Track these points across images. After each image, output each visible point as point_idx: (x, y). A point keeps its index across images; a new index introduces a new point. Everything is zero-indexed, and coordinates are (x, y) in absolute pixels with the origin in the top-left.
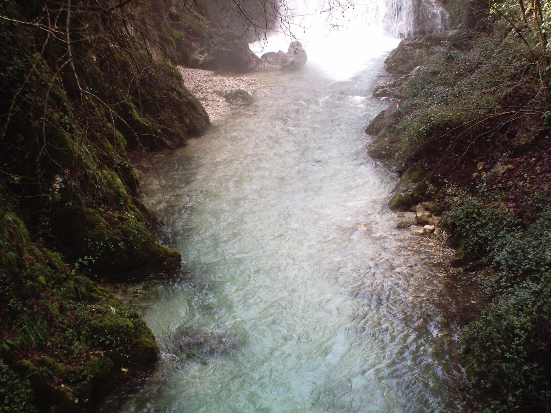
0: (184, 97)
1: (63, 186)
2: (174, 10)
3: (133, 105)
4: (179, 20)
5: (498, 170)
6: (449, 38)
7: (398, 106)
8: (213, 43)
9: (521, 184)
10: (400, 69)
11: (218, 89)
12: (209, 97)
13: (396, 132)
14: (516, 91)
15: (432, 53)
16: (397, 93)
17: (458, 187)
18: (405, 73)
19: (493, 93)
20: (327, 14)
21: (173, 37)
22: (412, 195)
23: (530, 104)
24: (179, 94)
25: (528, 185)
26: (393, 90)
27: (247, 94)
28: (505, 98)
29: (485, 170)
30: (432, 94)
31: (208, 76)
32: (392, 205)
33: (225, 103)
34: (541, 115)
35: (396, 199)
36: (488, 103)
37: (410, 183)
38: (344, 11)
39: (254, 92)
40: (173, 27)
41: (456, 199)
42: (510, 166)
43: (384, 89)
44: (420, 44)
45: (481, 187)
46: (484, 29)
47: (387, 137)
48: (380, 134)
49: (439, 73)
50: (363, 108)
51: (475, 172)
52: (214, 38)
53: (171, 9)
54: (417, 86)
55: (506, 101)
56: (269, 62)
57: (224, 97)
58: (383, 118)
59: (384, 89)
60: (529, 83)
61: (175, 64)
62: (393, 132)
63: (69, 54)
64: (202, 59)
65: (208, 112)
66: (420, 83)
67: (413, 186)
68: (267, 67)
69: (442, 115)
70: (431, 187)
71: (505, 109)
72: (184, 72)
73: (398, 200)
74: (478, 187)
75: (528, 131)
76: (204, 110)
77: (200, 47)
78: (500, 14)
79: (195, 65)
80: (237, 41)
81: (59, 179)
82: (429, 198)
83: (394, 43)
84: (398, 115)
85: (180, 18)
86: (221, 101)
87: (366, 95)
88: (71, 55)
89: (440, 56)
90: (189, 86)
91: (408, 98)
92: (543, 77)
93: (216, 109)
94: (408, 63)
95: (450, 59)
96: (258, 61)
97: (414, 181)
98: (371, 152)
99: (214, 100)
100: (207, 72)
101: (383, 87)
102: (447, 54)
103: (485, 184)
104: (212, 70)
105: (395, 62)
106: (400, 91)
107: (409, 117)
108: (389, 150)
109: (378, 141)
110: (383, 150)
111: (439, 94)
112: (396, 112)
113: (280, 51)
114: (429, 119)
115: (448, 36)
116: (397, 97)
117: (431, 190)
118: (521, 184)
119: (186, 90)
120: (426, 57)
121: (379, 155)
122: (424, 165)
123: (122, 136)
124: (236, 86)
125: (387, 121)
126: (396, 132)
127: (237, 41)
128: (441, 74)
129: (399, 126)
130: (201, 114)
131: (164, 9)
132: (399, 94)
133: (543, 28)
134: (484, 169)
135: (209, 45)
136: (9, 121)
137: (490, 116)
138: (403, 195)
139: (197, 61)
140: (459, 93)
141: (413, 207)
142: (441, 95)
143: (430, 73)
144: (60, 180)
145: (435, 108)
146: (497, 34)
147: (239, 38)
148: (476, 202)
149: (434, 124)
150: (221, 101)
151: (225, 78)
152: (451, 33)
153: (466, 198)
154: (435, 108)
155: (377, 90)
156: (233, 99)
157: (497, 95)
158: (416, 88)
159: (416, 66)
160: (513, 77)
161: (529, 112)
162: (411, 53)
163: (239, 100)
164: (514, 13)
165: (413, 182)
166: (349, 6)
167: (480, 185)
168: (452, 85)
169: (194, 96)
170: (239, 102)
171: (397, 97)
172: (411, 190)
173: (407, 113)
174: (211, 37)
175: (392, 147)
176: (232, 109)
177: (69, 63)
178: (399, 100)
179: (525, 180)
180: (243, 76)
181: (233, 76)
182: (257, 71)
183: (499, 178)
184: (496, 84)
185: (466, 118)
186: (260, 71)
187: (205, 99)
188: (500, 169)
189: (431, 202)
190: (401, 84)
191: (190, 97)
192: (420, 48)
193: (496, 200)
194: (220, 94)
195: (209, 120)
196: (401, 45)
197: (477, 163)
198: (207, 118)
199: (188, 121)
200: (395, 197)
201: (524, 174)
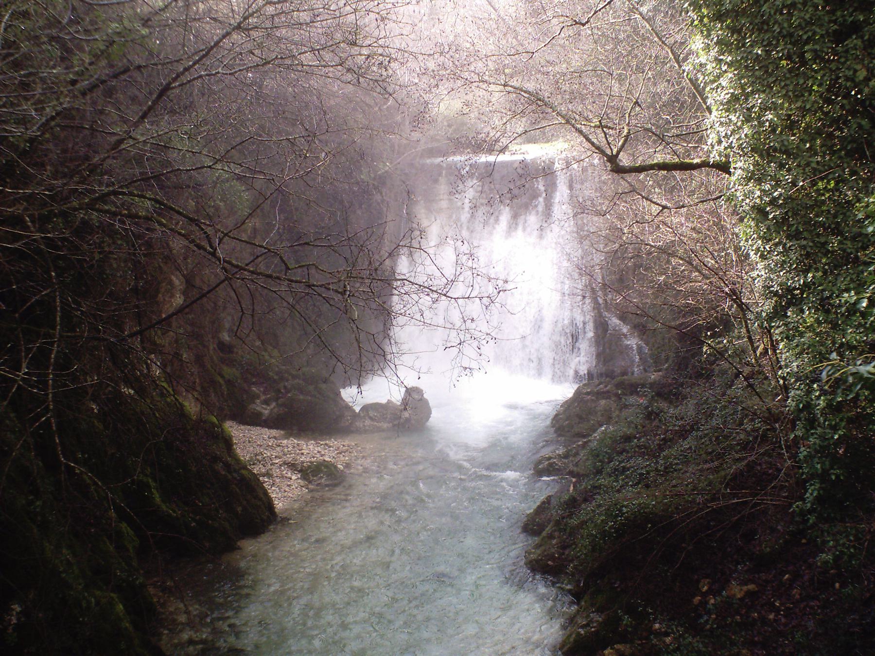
0: (235, 471)
1: (23, 619)
2: (226, 337)
3: (153, 484)
4: (232, 352)
5: (733, 592)
6: (651, 384)
7: (572, 488)
8: (285, 387)
9: (771, 616)
10: (576, 429)
11: (289, 458)
12: (276, 472)
13: (568, 531)
14: (750, 466)
15: (626, 406)
16: (571, 467)
17: (669, 620)
18: (584, 436)
19: (716, 470)
20: (456, 350)
21: (222, 377)
22: (597, 632)
23: (773, 488)
24: (227, 466)
25: (783, 620)
26: (565, 463)
27: (336, 467)
28: (735, 477)
29: (715, 593)
30: (625, 469)
31: (275, 438)
32: (565, 649)
33: (299, 481)
34: (790, 506)
35: (572, 640)
36: (710, 484)
37: (593, 612)
38: (482, 347)
39: (348, 466)
40: (223, 363)
41: (668, 640)
42: (751, 587)
43: (552, 461)
44: (608, 392)
45: (709, 621)
46: (699, 375)
47: (554, 538)
48: (544, 534)
49: (635, 438)
50: (518, 492)
51: (697, 596)
52: (287, 380)
53: (220, 335)
54: (601, 457)
55: (737, 482)
56: (371, 418)
57: (299, 471)
58: (548, 508)
59: (552, 461)
60: (770, 456)
61: (223, 418)
62: (565, 530)
63: (49, 405)
64: (266, 412)
65: (273, 496)
66: (606, 452)
67: (597, 618)
68: (369, 426)
69: (640, 504)
70: (626, 620)
71: (735, 496)
72: (236, 431)
73: (575, 641)
74: (702, 621)
75: (773, 530)
76: (266, 493)
77: (264, 393)
78: (720, 354)
79: (255, 420)
80: (323, 386)
81: (17, 608)
82: (623, 638)
83: (566, 391)
84: (572, 504)
85: (235, 350)
86: (294, 477)
87: (522, 471)
88: (51, 407)
89: (637, 411)
90: (243, 453)
91: (587, 476)
92: (788, 448)
93: (285, 491)
94: (588, 421)
95: (651, 415)
96: (355, 416)
97: (599, 611)
98: (531, 562)
99: (282, 477)
100: (274, 432)
101: (550, 458)
102: (647, 407)
103: (714, 616)
104: (282, 429)
105: (568, 419)
106: (576, 465)
107: (590, 507)
108: (559, 558)
109: (541, 546)
110: (549, 560)
111: (635, 471)
112: (569, 499)
113: (389, 402)
114: (620, 510)
115: (650, 381)
116: (571, 474)
117: (626, 625)
118: (771, 616)
119: (238, 460)
120: (617, 412)
121: (544, 567)
122: (615, 583)
123: (131, 533)
124: (318, 455)
125: (555, 513)
126: (568, 531)
127: (323, 386)
128: (639, 439)
129: (574, 522)
130: (260, 499)
131: (210, 336)
132: (575, 469)
133: (780, 377)
134: (710, 592)
135: (279, 391)
136: (136, 392)
137: (714, 505)
138: (583, 632)
139: (259, 414)
140: (666, 468)
141: (600, 652)
142: (639, 471)
143: (622, 437)
144: (19, 609)
145: (629, 492)
146: (718, 381)
147: (325, 381)
148: (701, 645)
149: (626, 519)
150: (294, 477)
151: (302, 442)
152: (654, 377)
153: (684, 639)
154: (629, 492)
155: (540, 462)
156: (313, 476)
157: (723, 473)
158: (600, 461)
159: (601, 426)
160: (745, 446)
161: (771, 500)
162: (593, 405)
163: (322, 477)
164: (741, 353)
165: (597, 611)
166: (489, 340)
167: (705, 618)
168: (654, 455)
169: (250, 471)
170: (323, 481)
171: (571, 474)
172: (595, 625)
173: (585, 500)
174: (282, 379)
175: (563, 554)
176: (311, 491)
177: (48, 419)
178: (574, 480)
179: (777, 611)
180: (330, 439)
181: (315, 439)
182: (352, 432)
183: (736, 606)
184: (720, 456)
185: (677, 508)
186: (358, 431)
187: (268, 474)
188: (737, 590)
189: (628, 646)
190: (577, 454)
191: (244, 472)
192: (607, 398)
193: (733, 643)
194: (292, 466)
195: (274, 508)
196: (578, 393)
197: (698, 581)
198: (270, 506)
199: (239, 509)
200: (570, 635)
201: (775, 601)
